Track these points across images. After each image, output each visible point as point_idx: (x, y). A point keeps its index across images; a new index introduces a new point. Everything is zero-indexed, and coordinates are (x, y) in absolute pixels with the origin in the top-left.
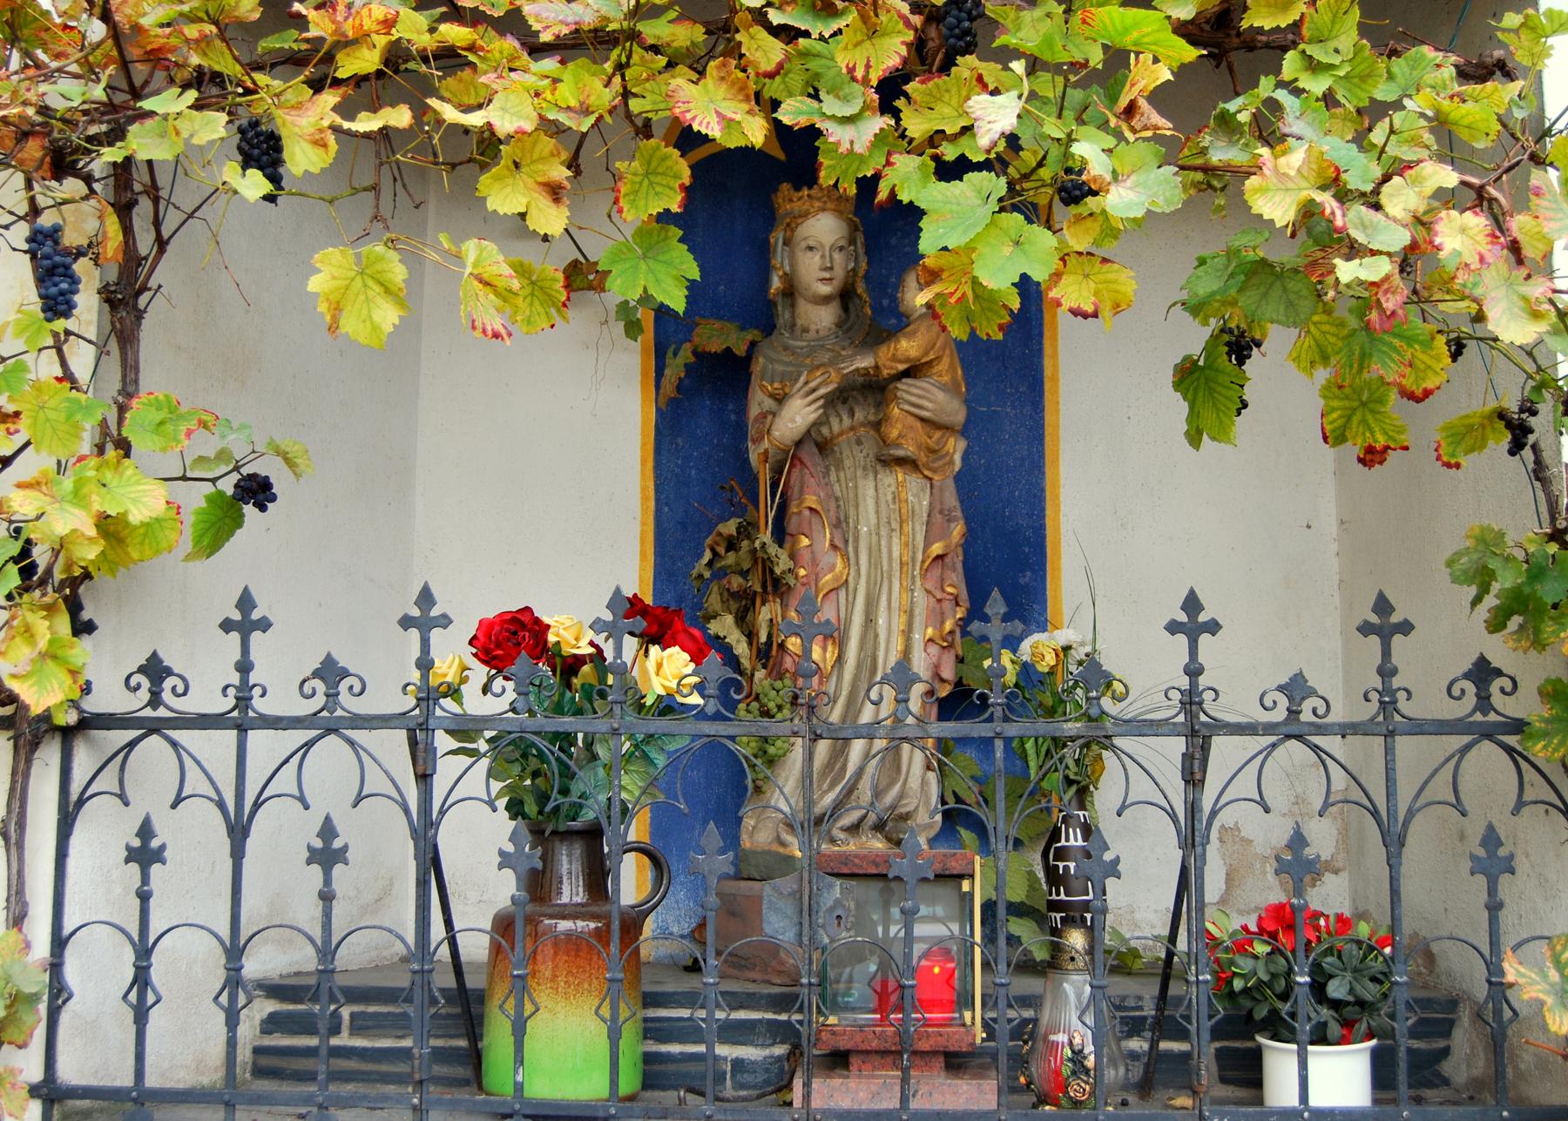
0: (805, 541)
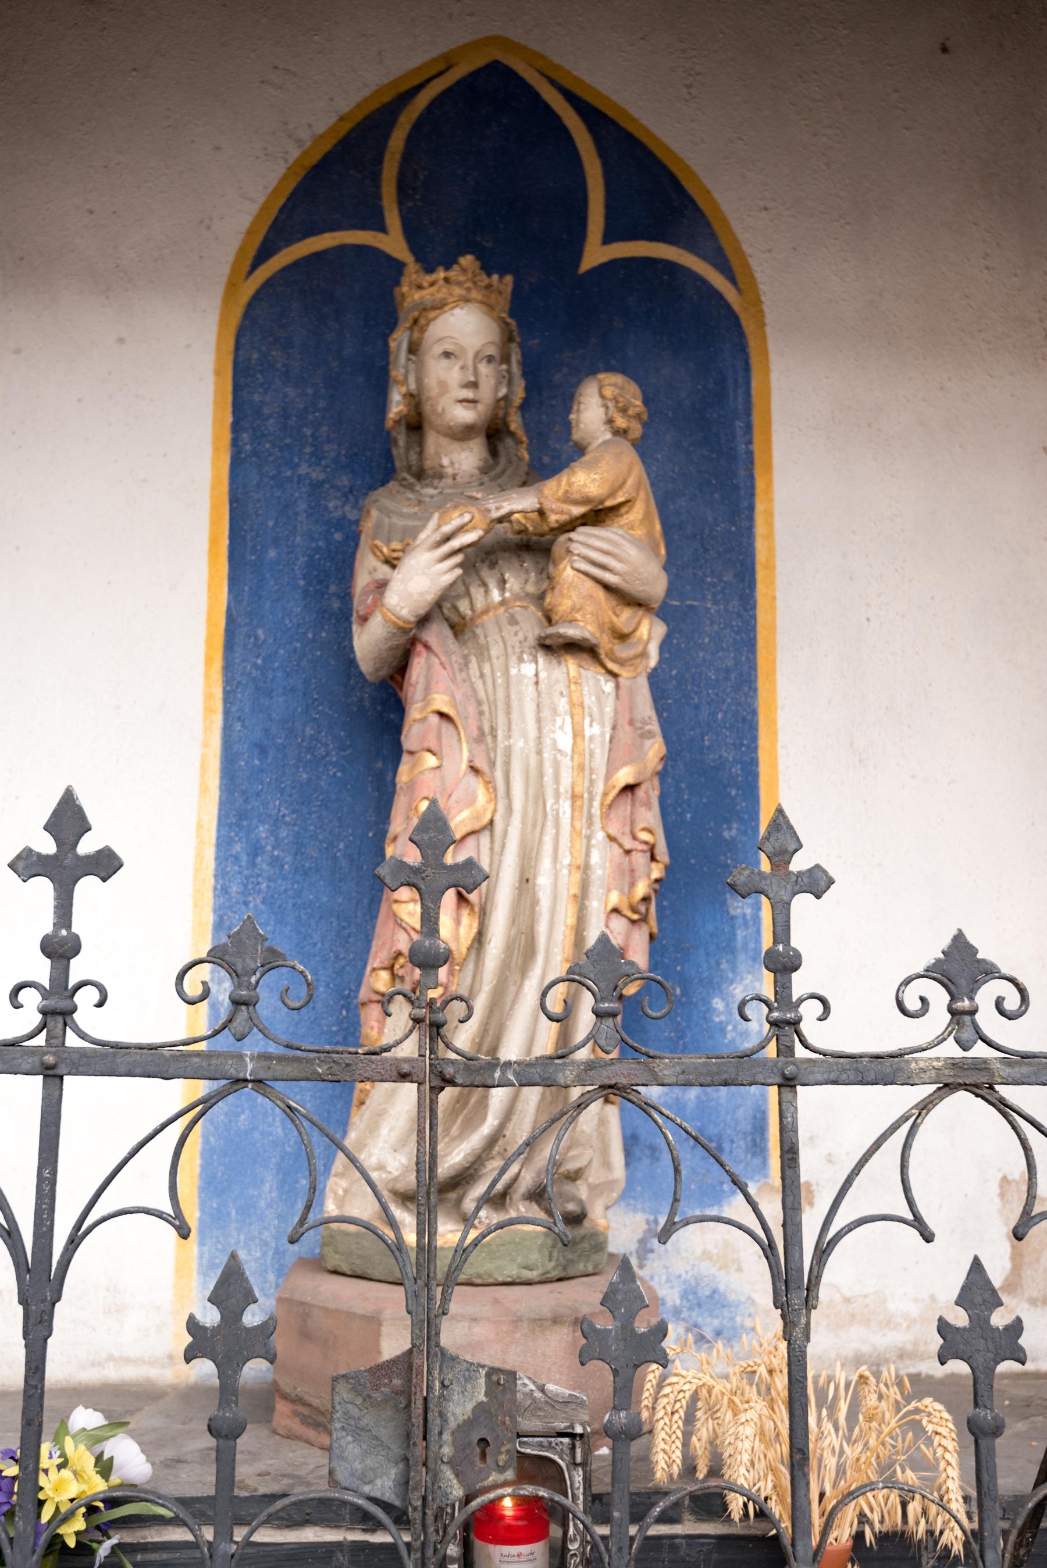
0: (431, 761)
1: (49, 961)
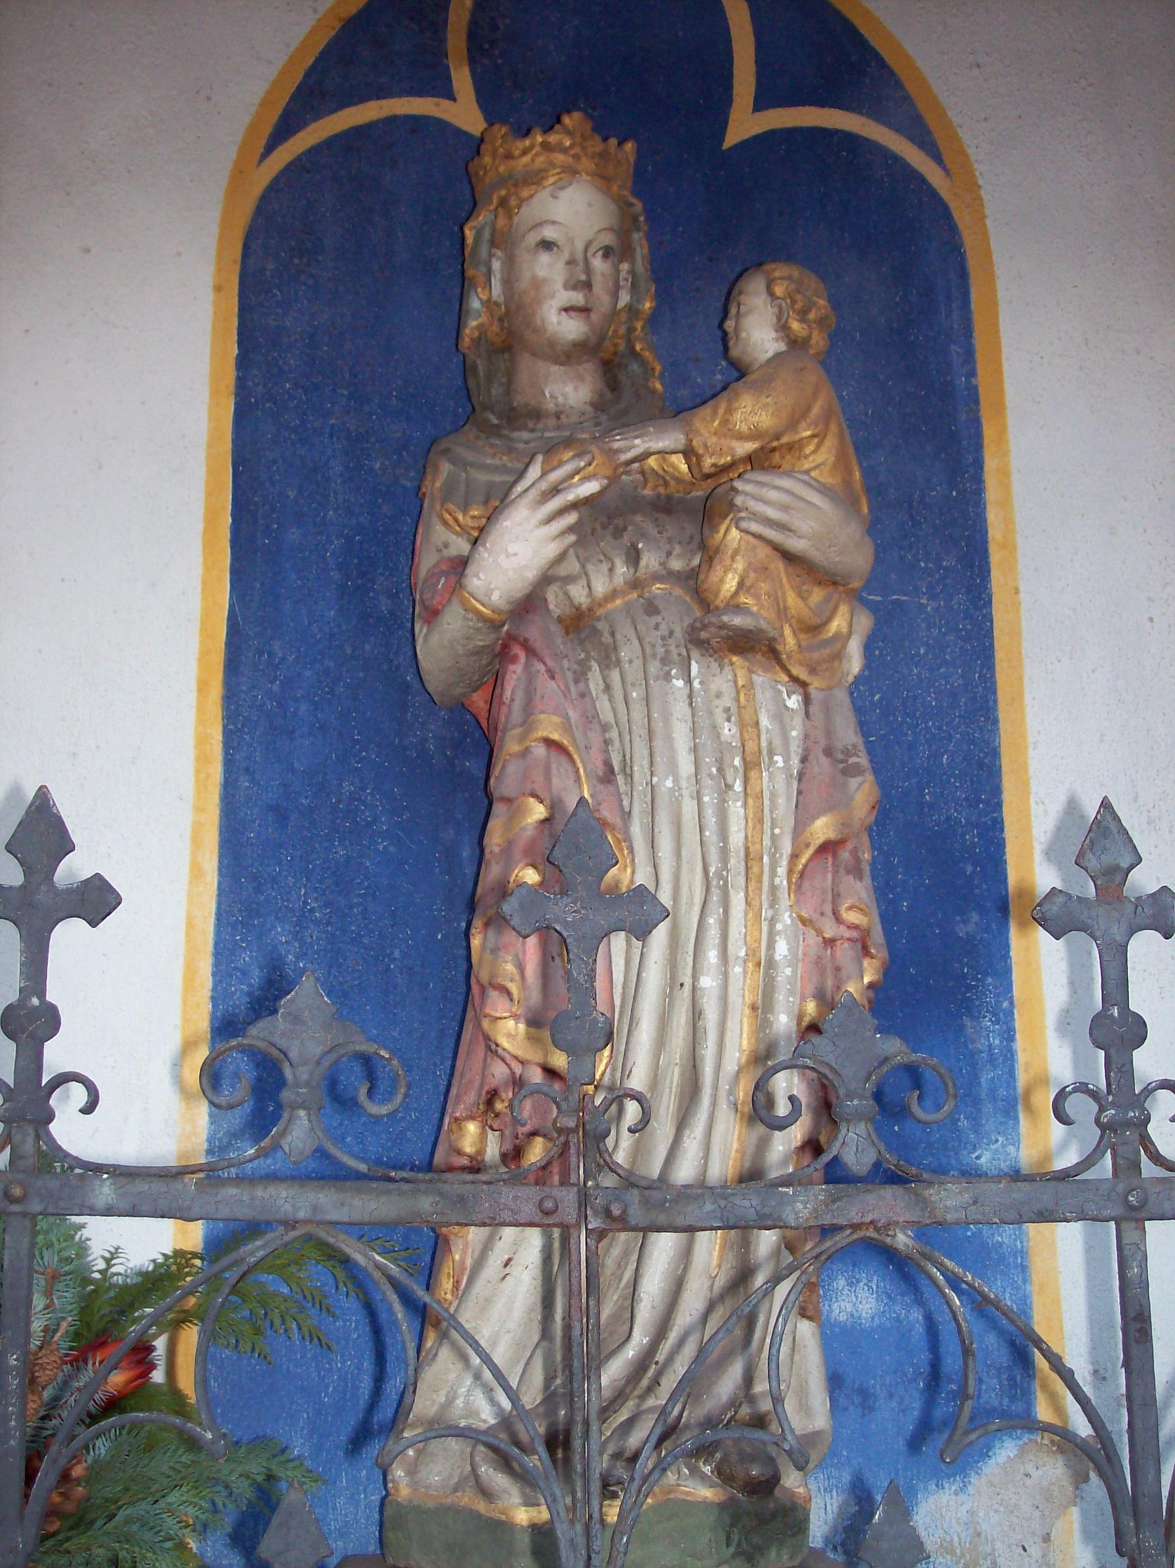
1: (12, 1047)
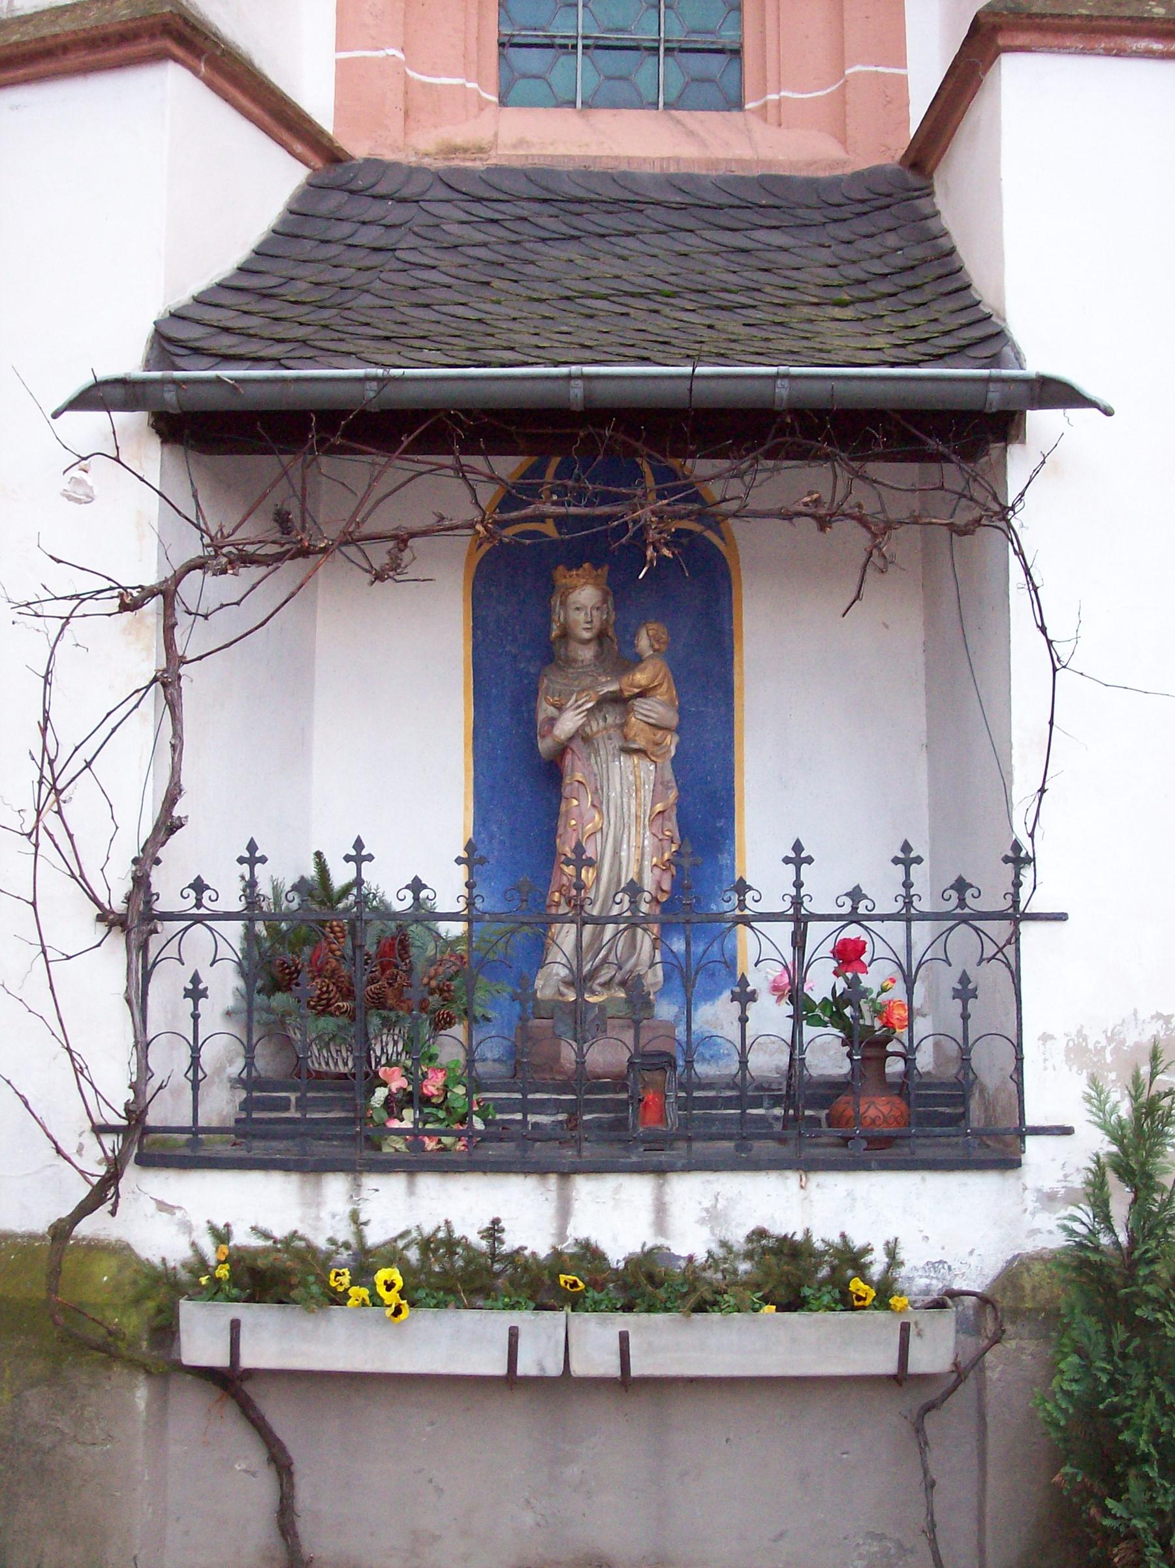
0: (575, 802)
